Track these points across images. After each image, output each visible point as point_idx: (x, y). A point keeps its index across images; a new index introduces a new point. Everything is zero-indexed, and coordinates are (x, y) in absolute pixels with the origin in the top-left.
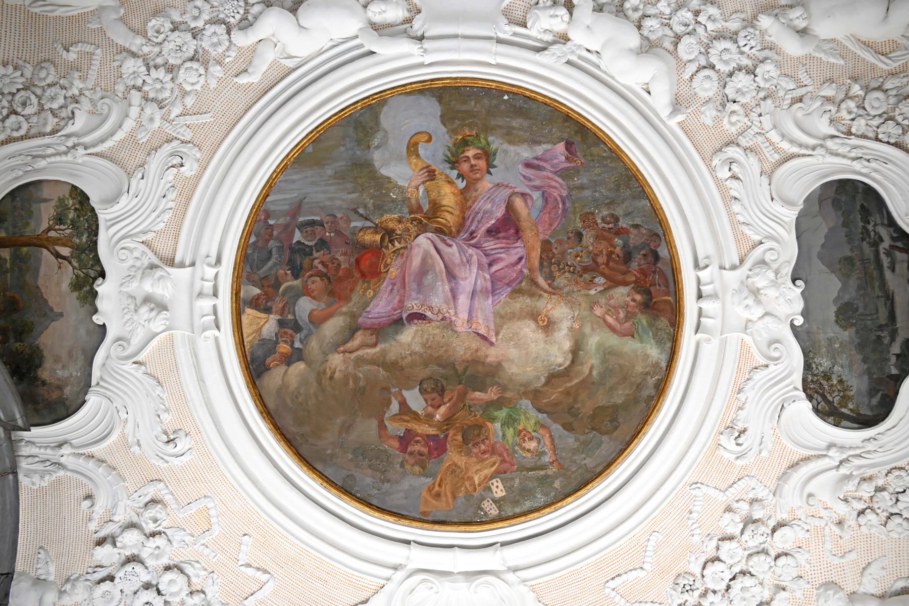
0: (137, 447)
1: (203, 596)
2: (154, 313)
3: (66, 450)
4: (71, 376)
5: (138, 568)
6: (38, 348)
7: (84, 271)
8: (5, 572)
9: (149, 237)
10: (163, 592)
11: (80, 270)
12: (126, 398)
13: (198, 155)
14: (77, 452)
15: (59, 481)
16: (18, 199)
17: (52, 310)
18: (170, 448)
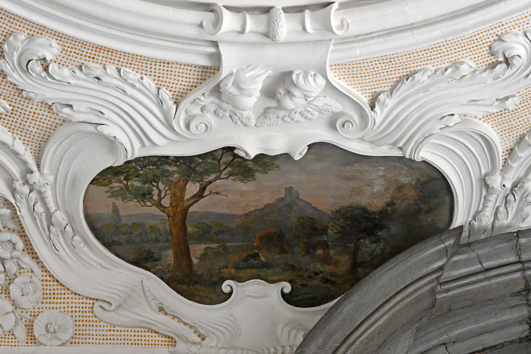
2: (296, 92)
3: (496, 181)
6: (337, 211)
9: (166, 95)
11: (221, 173)
13: (22, 37)
14: (501, 168)
16: (117, 238)
17: (282, 199)
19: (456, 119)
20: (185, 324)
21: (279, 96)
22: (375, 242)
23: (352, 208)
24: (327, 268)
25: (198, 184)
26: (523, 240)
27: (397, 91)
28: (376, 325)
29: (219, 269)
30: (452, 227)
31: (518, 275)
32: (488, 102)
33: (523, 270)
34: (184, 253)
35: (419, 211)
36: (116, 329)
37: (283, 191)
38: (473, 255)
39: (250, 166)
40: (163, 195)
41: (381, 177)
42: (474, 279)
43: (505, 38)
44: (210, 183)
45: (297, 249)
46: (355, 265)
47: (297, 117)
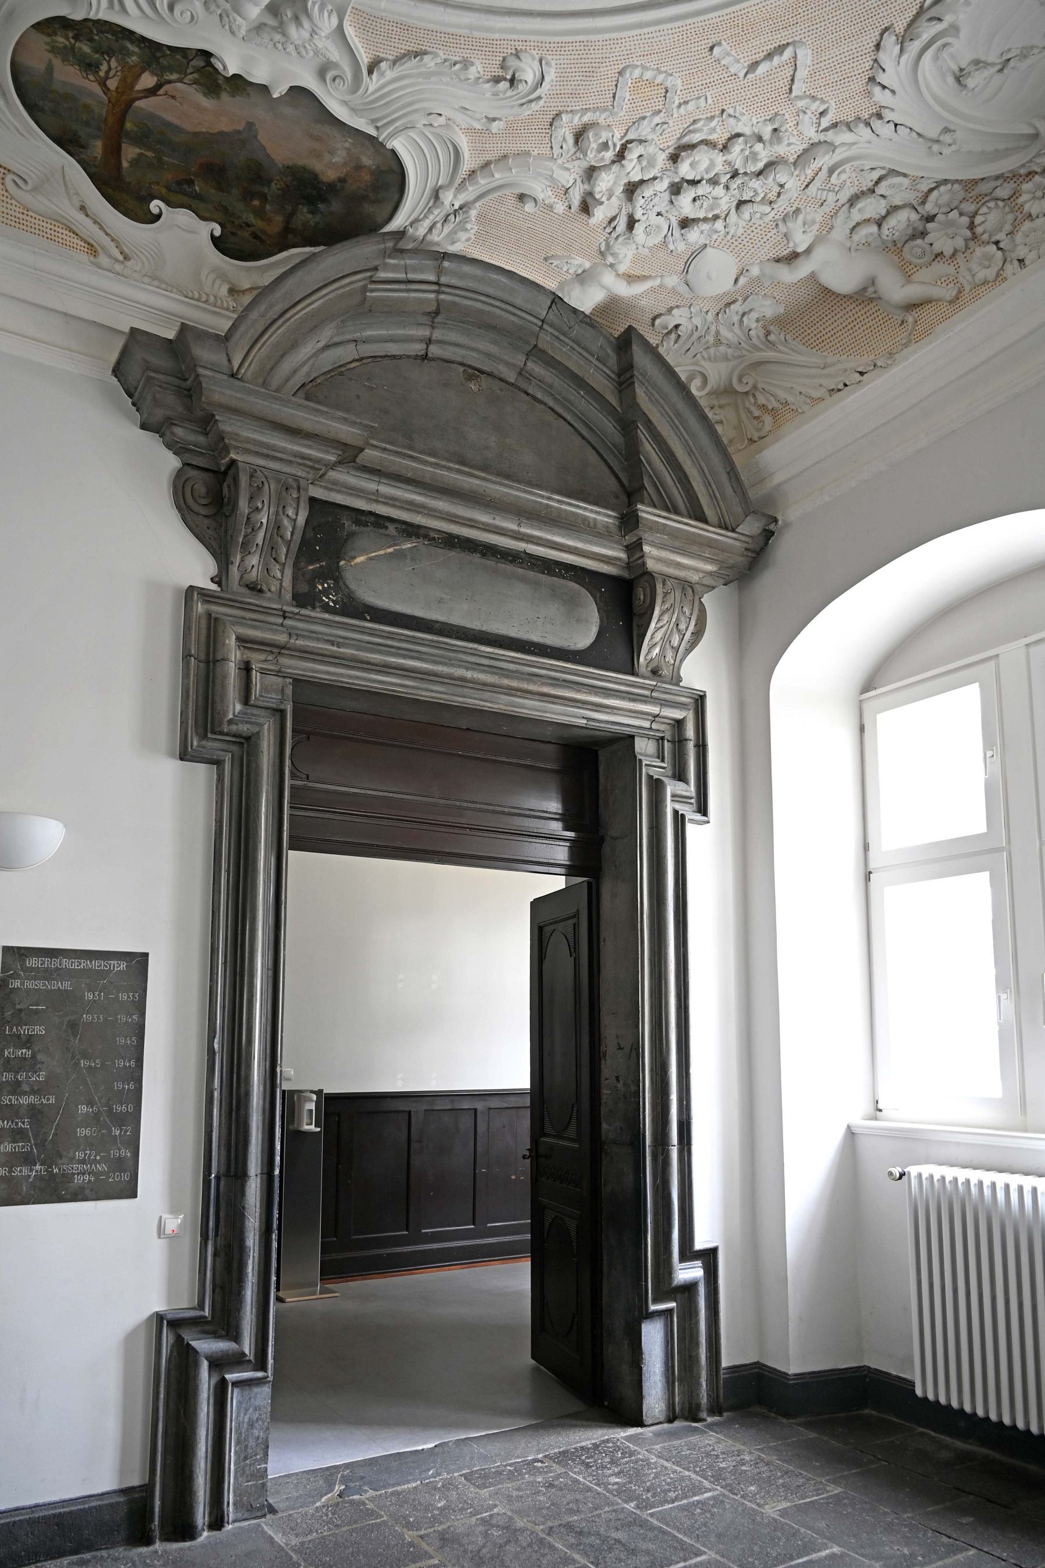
0: (495, 124)
1: (741, 139)
2: (306, 24)
3: (448, 197)
4: (349, 149)
5: (648, 191)
6: (288, 167)
7: (189, 71)
8: (549, 303)
10: (698, 178)
11: (186, 75)
12: (417, 106)
15: (479, 216)
16: (41, 103)
17: (239, 132)
18: (522, 88)
19: (442, 120)
20: (107, 234)
21: (284, 17)
22: (312, 212)
23: (304, 169)
24: (260, 224)
25: (156, 79)
26: (446, 264)
27: (401, 65)
28: (311, 307)
29: (150, 183)
30: (388, 229)
31: (432, 296)
32: (478, 116)
33: (438, 292)
34: (114, 151)
35: (365, 198)
36: (30, 213)
37: (244, 124)
38: (402, 262)
39: (220, 82)
40: (111, 74)
41: (345, 148)
42: (396, 286)
43: (522, 55)
44: (170, 82)
45: (235, 191)
46: (287, 229)
47: (291, 48)
